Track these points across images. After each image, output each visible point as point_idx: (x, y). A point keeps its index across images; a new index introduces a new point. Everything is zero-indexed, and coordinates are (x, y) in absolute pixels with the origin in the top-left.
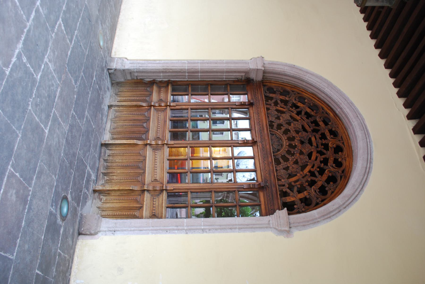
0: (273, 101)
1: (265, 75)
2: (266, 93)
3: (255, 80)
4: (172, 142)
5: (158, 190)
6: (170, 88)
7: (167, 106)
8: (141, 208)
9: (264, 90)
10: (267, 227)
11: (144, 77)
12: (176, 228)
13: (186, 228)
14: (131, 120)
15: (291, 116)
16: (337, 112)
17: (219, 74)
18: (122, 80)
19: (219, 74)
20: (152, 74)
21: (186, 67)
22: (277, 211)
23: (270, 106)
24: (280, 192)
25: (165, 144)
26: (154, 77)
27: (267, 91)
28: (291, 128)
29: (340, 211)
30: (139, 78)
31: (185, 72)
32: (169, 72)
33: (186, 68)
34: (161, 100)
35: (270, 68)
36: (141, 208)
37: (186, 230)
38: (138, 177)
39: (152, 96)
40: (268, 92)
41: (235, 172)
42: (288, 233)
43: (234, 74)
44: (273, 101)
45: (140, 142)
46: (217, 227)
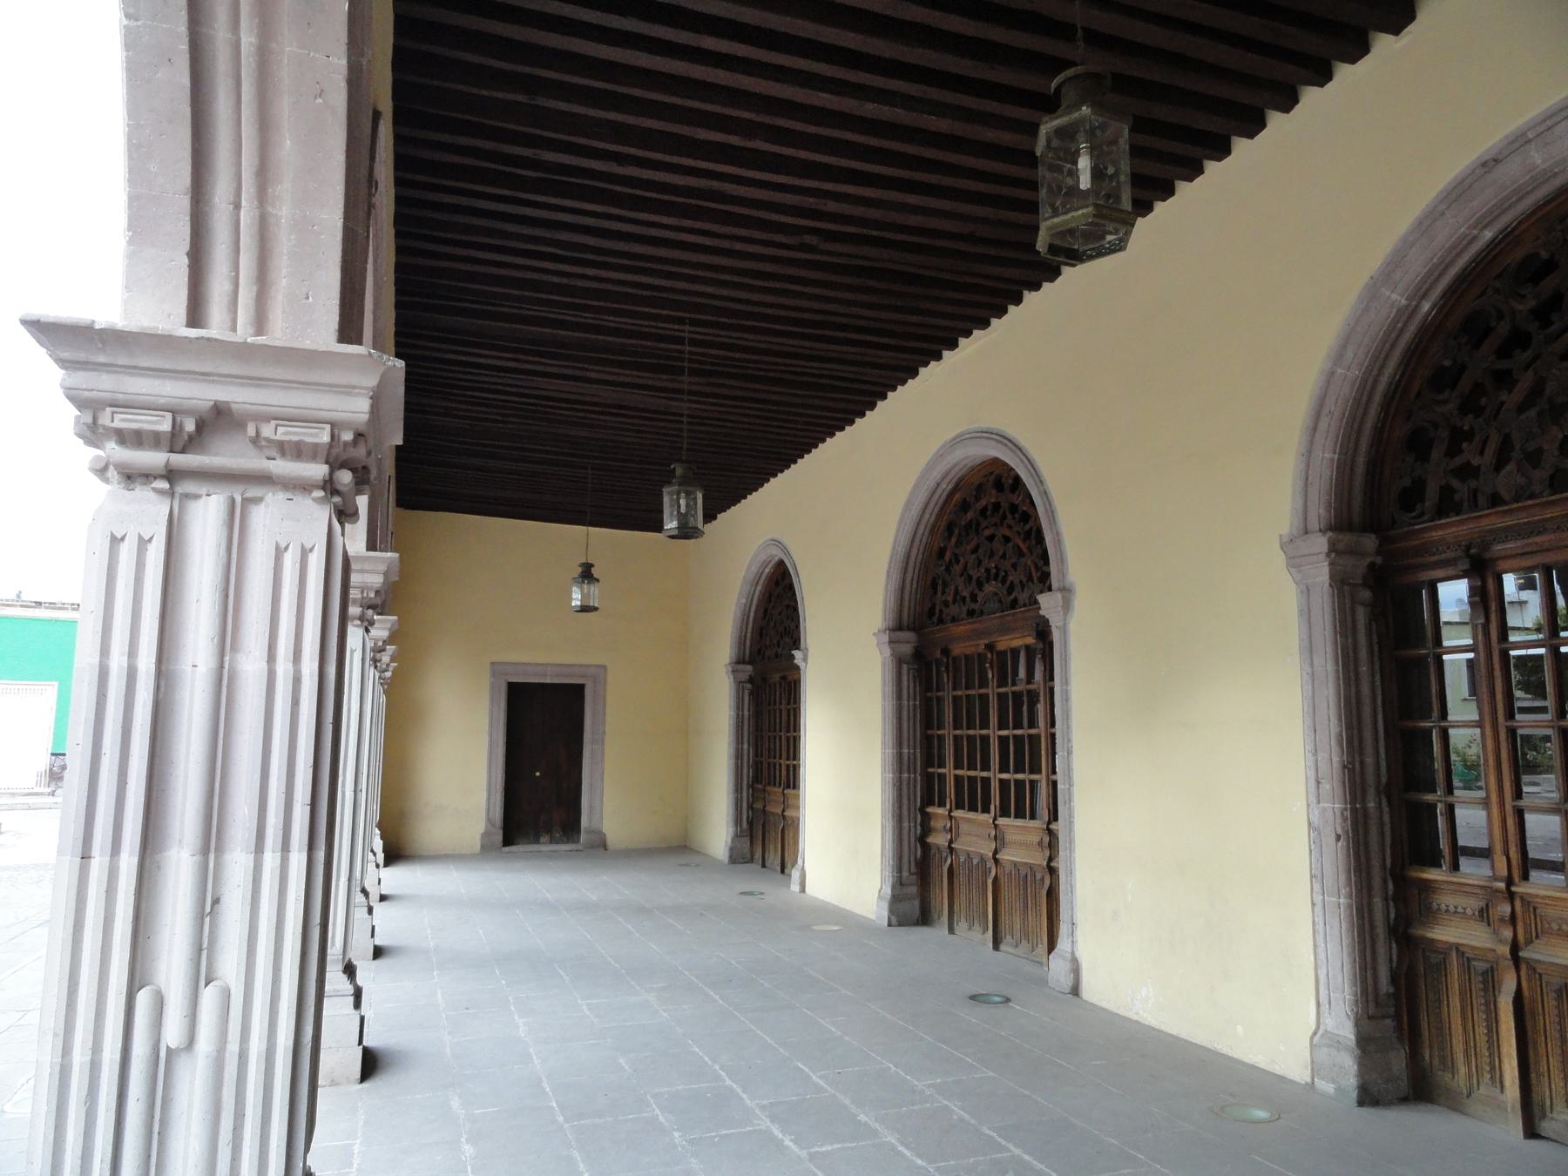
0: (1455, 483)
1: (905, 624)
2: (1422, 514)
3: (915, 644)
4: (948, 806)
5: (1050, 840)
6: (930, 810)
7: (1511, 896)
8: (1463, 953)
9: (1412, 521)
10: (1065, 632)
11: (912, 859)
12: (1067, 806)
13: (1067, 786)
14: (969, 890)
15: (1522, 408)
16: (950, 487)
17: (905, 714)
18: (917, 903)
19: (905, 714)
20: (905, 843)
21: (1336, 806)
22: (1041, 612)
23: (1479, 494)
24: (1451, 514)
25: (994, 822)
26: (913, 839)
27: (1414, 510)
28: (974, 574)
29: (1045, 492)
30: (913, 869)
31: (900, 780)
32: (900, 807)
33: (891, 775)
34: (1484, 915)
35: (1319, 512)
36: (1463, 953)
37: (1070, 786)
38: (1475, 969)
39: (1462, 945)
40: (1419, 506)
41: (1557, 641)
42: (1067, 591)
43: (905, 683)
44: (1455, 483)
45: (1509, 985)
46: (1065, 726)
